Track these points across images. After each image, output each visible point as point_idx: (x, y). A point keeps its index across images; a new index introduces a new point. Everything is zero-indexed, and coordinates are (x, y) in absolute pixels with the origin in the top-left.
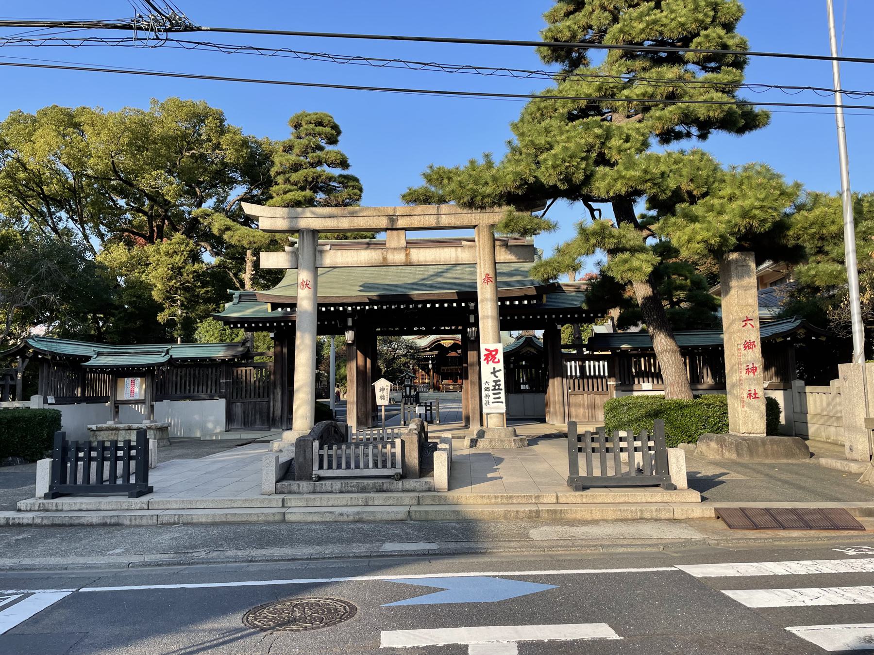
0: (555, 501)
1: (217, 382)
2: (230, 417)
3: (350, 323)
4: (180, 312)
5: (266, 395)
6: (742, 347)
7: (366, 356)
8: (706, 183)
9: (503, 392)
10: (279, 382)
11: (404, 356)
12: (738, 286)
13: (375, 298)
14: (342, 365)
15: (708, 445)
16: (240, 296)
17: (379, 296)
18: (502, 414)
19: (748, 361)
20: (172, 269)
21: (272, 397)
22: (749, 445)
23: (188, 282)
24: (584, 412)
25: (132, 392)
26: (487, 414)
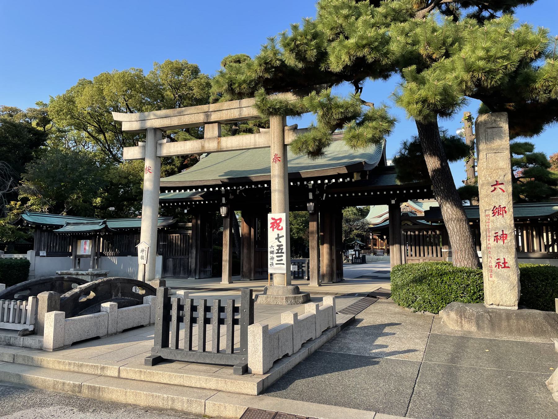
0: (116, 374)
6: (491, 213)
8: (444, 44)
9: (284, 255)
10: (194, 244)
12: (487, 149)
15: (448, 315)
17: (228, 179)
18: (284, 274)
19: (497, 228)
22: (495, 319)
25: (85, 249)
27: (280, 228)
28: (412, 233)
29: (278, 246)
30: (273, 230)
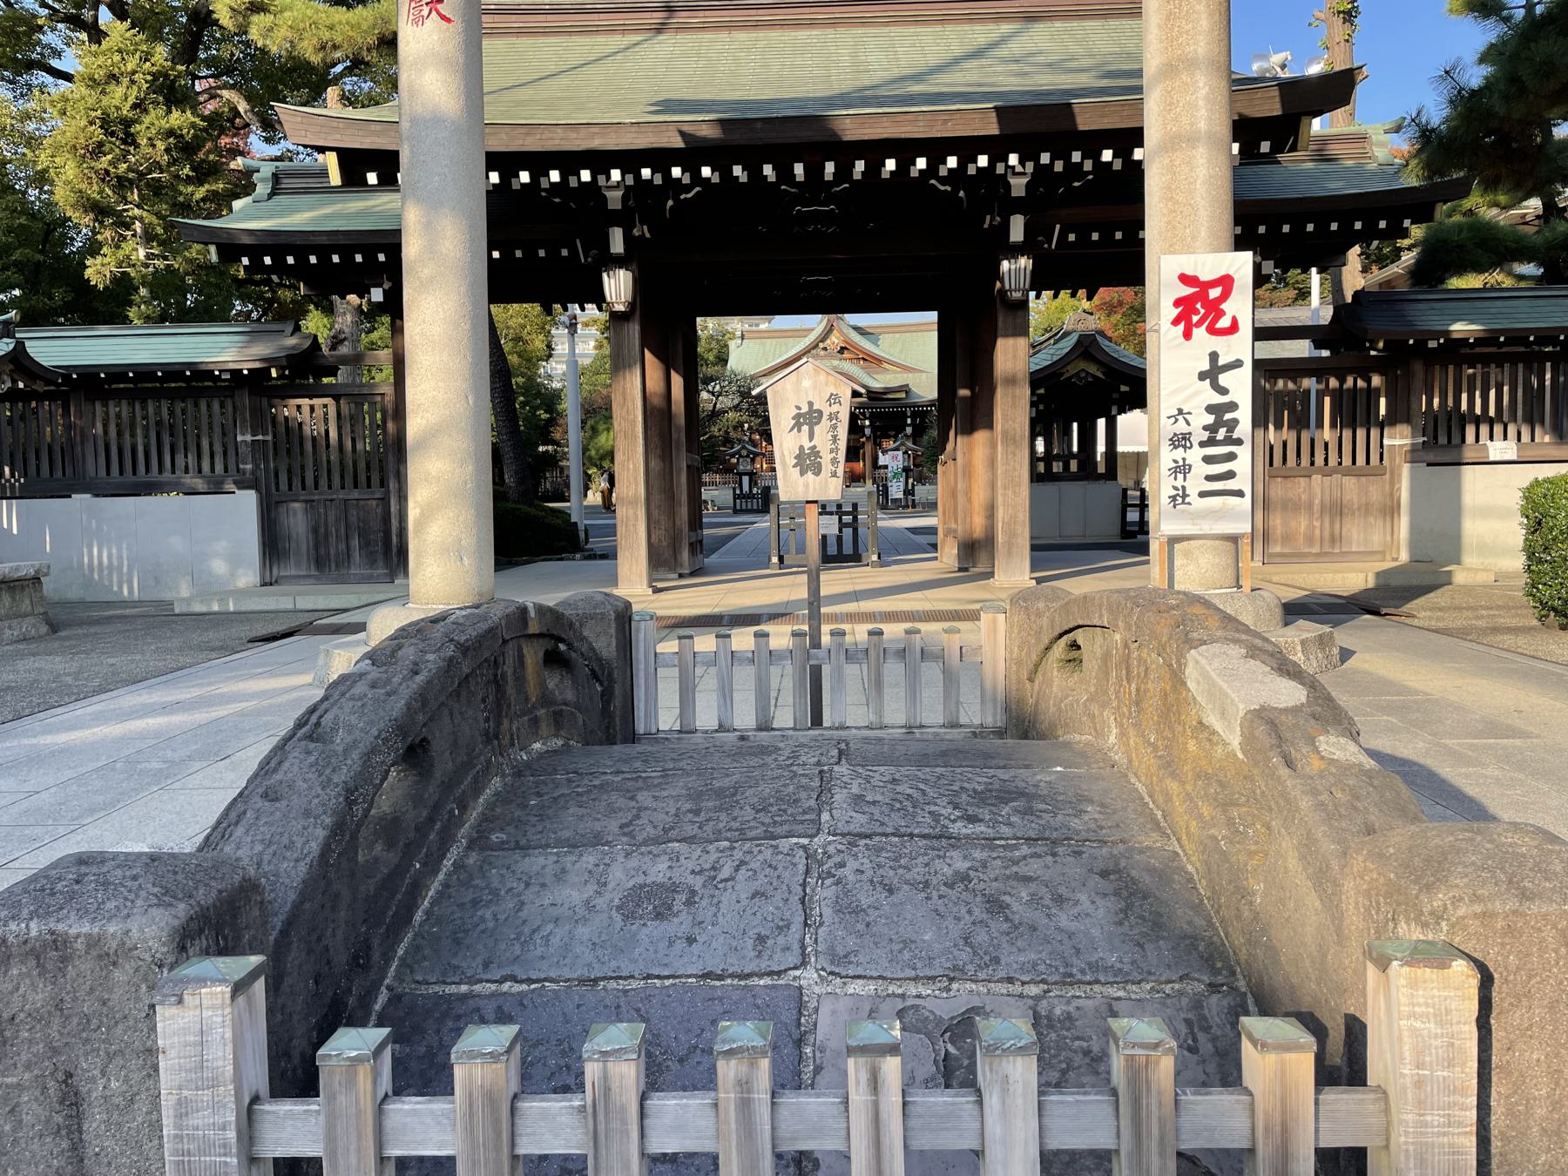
1: (230, 449)
2: (273, 545)
3: (617, 244)
4: (142, 253)
7: (668, 365)
11: (736, 408)
13: (707, 132)
14: (601, 427)
16: (276, 177)
20: (105, 123)
21: (392, 485)
23: (157, 166)
24: (1311, 527)
26: (1173, 540)
27: (1224, 323)
28: (1361, 383)
29: (1210, 409)
30: (1187, 335)
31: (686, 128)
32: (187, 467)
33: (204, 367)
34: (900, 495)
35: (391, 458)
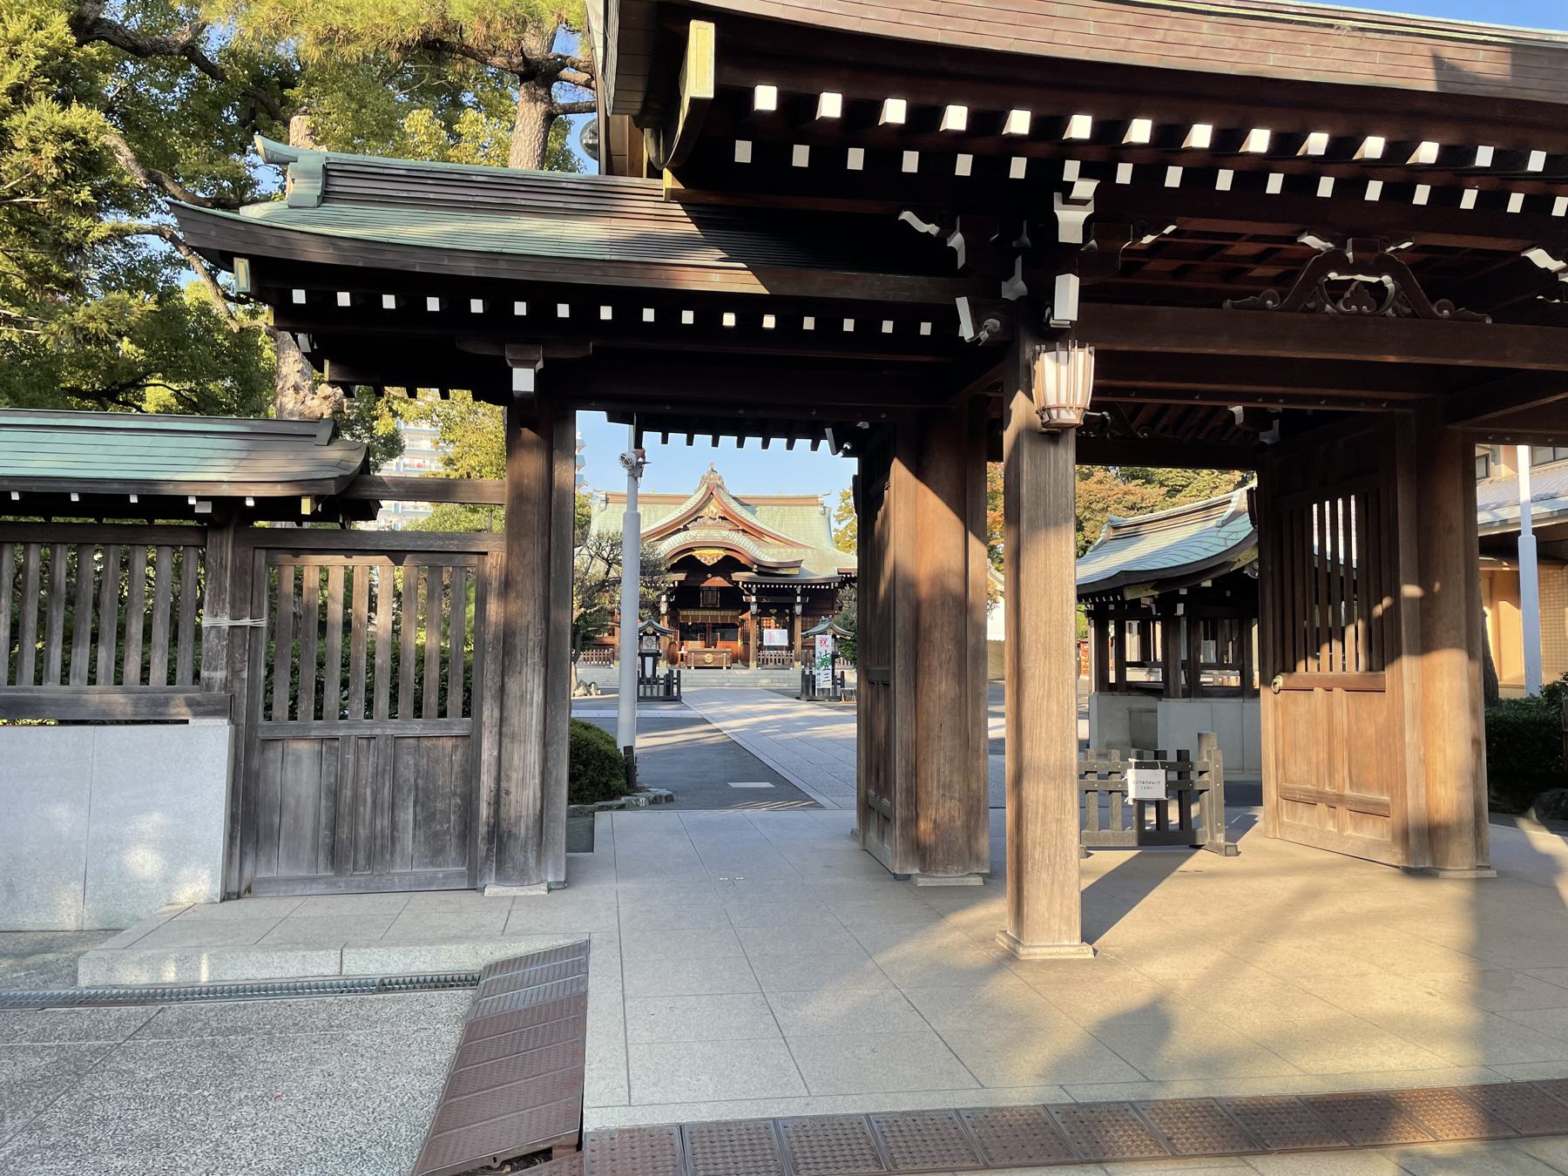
2: (250, 820)
5: (455, 698)
21: (489, 713)
31: (1449, 52)
32: (92, 671)
33: (169, 490)
34: (829, 685)
35: (490, 667)
